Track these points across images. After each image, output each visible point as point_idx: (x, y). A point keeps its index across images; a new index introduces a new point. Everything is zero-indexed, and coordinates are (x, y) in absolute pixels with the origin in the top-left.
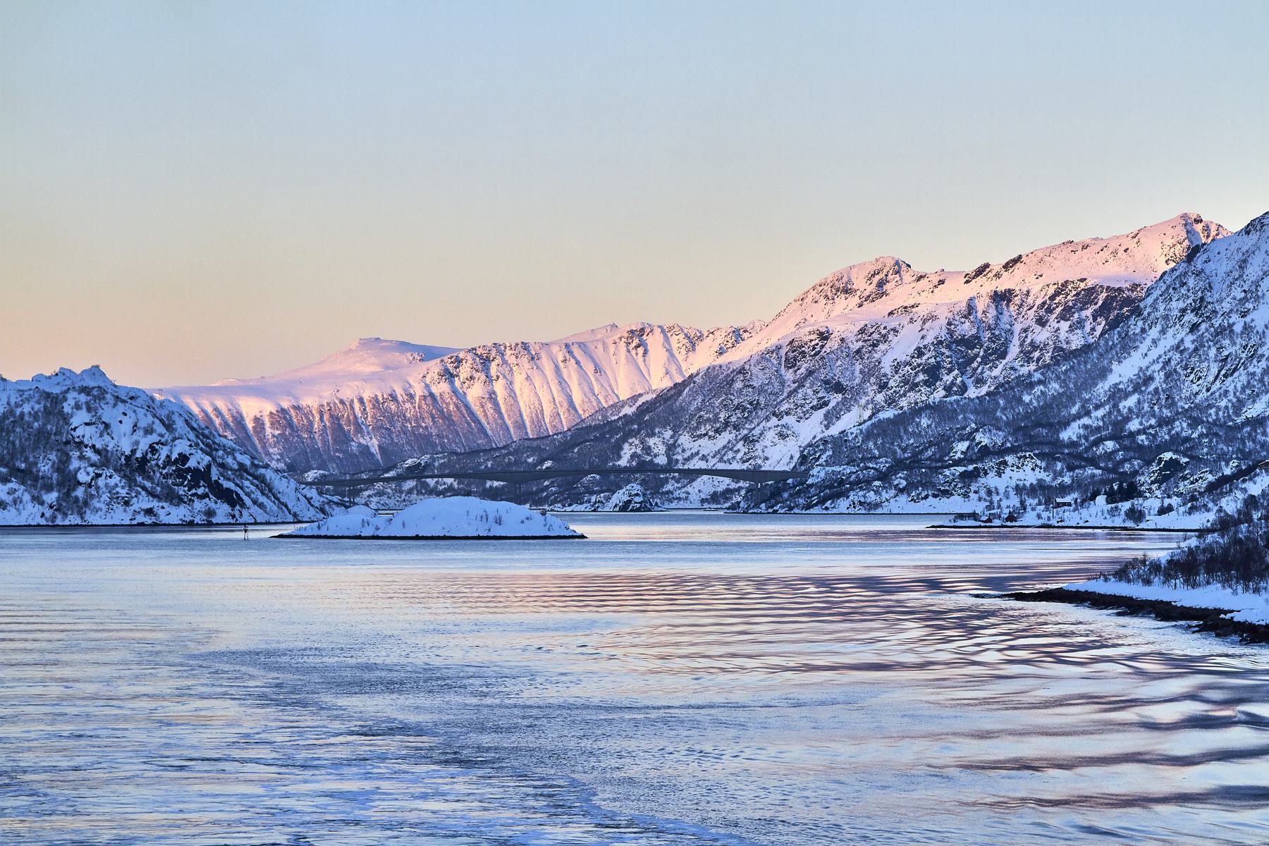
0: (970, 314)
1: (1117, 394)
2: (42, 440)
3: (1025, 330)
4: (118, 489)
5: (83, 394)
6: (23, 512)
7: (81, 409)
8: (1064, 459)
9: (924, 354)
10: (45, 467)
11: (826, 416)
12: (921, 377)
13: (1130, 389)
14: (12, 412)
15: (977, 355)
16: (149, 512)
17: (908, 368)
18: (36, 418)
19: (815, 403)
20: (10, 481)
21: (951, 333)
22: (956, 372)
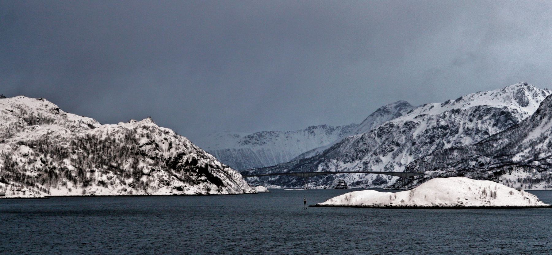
0: (445, 117)
1: (533, 144)
2: (123, 152)
3: (465, 124)
4: (164, 177)
5: (145, 129)
6: (116, 188)
7: (144, 136)
8: (536, 168)
9: (429, 132)
10: (126, 166)
11: (393, 154)
12: (428, 140)
13: (538, 141)
14: (109, 138)
15: (447, 133)
16: (179, 189)
17: (423, 137)
18: (121, 141)
19: (389, 150)
20: (109, 173)
21: (438, 124)
22: (440, 139)
